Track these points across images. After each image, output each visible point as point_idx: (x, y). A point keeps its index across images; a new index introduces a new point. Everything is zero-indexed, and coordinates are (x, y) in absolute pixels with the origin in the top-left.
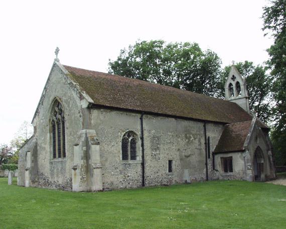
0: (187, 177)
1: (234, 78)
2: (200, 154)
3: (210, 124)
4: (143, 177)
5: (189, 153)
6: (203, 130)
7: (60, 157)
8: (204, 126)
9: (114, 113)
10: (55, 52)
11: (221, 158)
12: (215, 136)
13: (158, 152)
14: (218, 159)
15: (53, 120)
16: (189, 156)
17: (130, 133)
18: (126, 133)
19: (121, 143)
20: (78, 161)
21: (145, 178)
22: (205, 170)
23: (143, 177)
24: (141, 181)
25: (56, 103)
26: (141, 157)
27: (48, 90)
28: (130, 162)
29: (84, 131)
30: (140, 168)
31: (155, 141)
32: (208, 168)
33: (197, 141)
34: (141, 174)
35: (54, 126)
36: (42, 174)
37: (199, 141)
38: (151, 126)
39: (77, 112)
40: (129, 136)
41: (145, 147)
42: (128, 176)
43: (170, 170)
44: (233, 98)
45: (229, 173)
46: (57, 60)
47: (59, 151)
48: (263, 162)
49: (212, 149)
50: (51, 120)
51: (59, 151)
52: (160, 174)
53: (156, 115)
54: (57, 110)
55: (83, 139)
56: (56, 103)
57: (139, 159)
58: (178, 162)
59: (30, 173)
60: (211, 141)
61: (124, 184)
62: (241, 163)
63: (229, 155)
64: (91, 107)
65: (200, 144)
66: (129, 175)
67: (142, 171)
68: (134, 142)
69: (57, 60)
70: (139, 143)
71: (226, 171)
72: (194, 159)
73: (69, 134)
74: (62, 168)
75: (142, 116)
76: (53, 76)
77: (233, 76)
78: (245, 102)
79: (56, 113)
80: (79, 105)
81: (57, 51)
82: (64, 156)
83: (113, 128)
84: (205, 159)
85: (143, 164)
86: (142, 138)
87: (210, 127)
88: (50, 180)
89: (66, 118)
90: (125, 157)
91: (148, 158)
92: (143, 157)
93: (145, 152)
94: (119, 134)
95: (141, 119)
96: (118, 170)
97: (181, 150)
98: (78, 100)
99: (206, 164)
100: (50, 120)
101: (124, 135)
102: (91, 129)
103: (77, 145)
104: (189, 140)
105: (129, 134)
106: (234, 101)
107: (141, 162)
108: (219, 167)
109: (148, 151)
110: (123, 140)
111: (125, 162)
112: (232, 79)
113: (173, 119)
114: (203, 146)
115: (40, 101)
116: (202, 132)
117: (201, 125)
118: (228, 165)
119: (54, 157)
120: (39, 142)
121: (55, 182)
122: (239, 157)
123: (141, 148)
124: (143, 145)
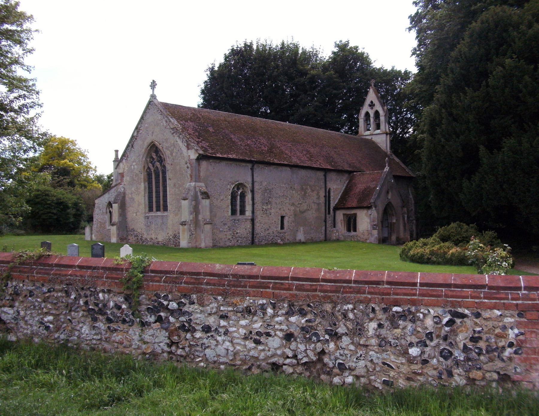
0: (301, 236)
1: (372, 105)
2: (318, 210)
3: (332, 173)
4: (253, 234)
5: (305, 208)
6: (324, 181)
7: (158, 210)
8: (325, 176)
9: (223, 163)
10: (151, 86)
11: (344, 215)
12: (337, 187)
13: (269, 207)
14: (340, 215)
15: (149, 168)
16: (304, 212)
17: (240, 186)
18: (236, 185)
19: (230, 197)
20: (186, 215)
21: (255, 236)
22: (324, 228)
23: (253, 234)
24: (250, 239)
25: (154, 150)
26: (251, 212)
27: (141, 131)
28: (241, 217)
29: (193, 184)
30: (249, 225)
31: (266, 194)
32: (327, 227)
33: (315, 194)
34: (250, 230)
35: (149, 175)
36: (133, 230)
37: (318, 194)
38: (264, 177)
39: (184, 163)
40: (238, 189)
41: (255, 201)
42: (237, 233)
43: (282, 227)
44: (368, 133)
45: (353, 233)
46: (153, 96)
47: (157, 201)
48: (394, 221)
49: (332, 205)
50: (146, 168)
51: (157, 201)
52: (270, 231)
53: (269, 164)
54: (154, 157)
55: (192, 193)
56: (154, 150)
57: (248, 213)
58: (292, 218)
59: (118, 229)
60: (332, 194)
61: (233, 242)
62: (365, 221)
63: (353, 212)
64: (201, 158)
65: (318, 198)
66: (238, 232)
67: (251, 227)
68: (243, 196)
69: (153, 96)
70: (249, 197)
71: (349, 230)
72: (311, 215)
73: (172, 185)
74: (163, 223)
75: (253, 166)
76: (148, 115)
77: (372, 102)
78: (385, 138)
79: (153, 159)
80: (185, 154)
81: (153, 85)
82: (165, 209)
83: (222, 181)
84: (323, 215)
85: (253, 220)
86: (253, 191)
87: (332, 176)
88: (145, 236)
89: (168, 167)
90: (234, 212)
91: (258, 213)
92: (253, 212)
93: (255, 206)
94: (229, 187)
95: (252, 169)
96: (226, 227)
97: (296, 204)
98: (184, 149)
99: (325, 221)
100: (144, 167)
101: (234, 188)
102: (200, 182)
103: (185, 199)
104: (305, 193)
105: (238, 186)
106: (369, 138)
107: (250, 218)
108: (341, 226)
109: (258, 206)
110: (232, 193)
111: (234, 217)
112: (370, 106)
113: (288, 169)
114: (322, 200)
115: (130, 142)
116: (322, 184)
117: (321, 174)
118: (351, 224)
119: (151, 209)
120: (128, 192)
121: (152, 239)
122: (364, 214)
123: (251, 202)
124: (253, 199)
